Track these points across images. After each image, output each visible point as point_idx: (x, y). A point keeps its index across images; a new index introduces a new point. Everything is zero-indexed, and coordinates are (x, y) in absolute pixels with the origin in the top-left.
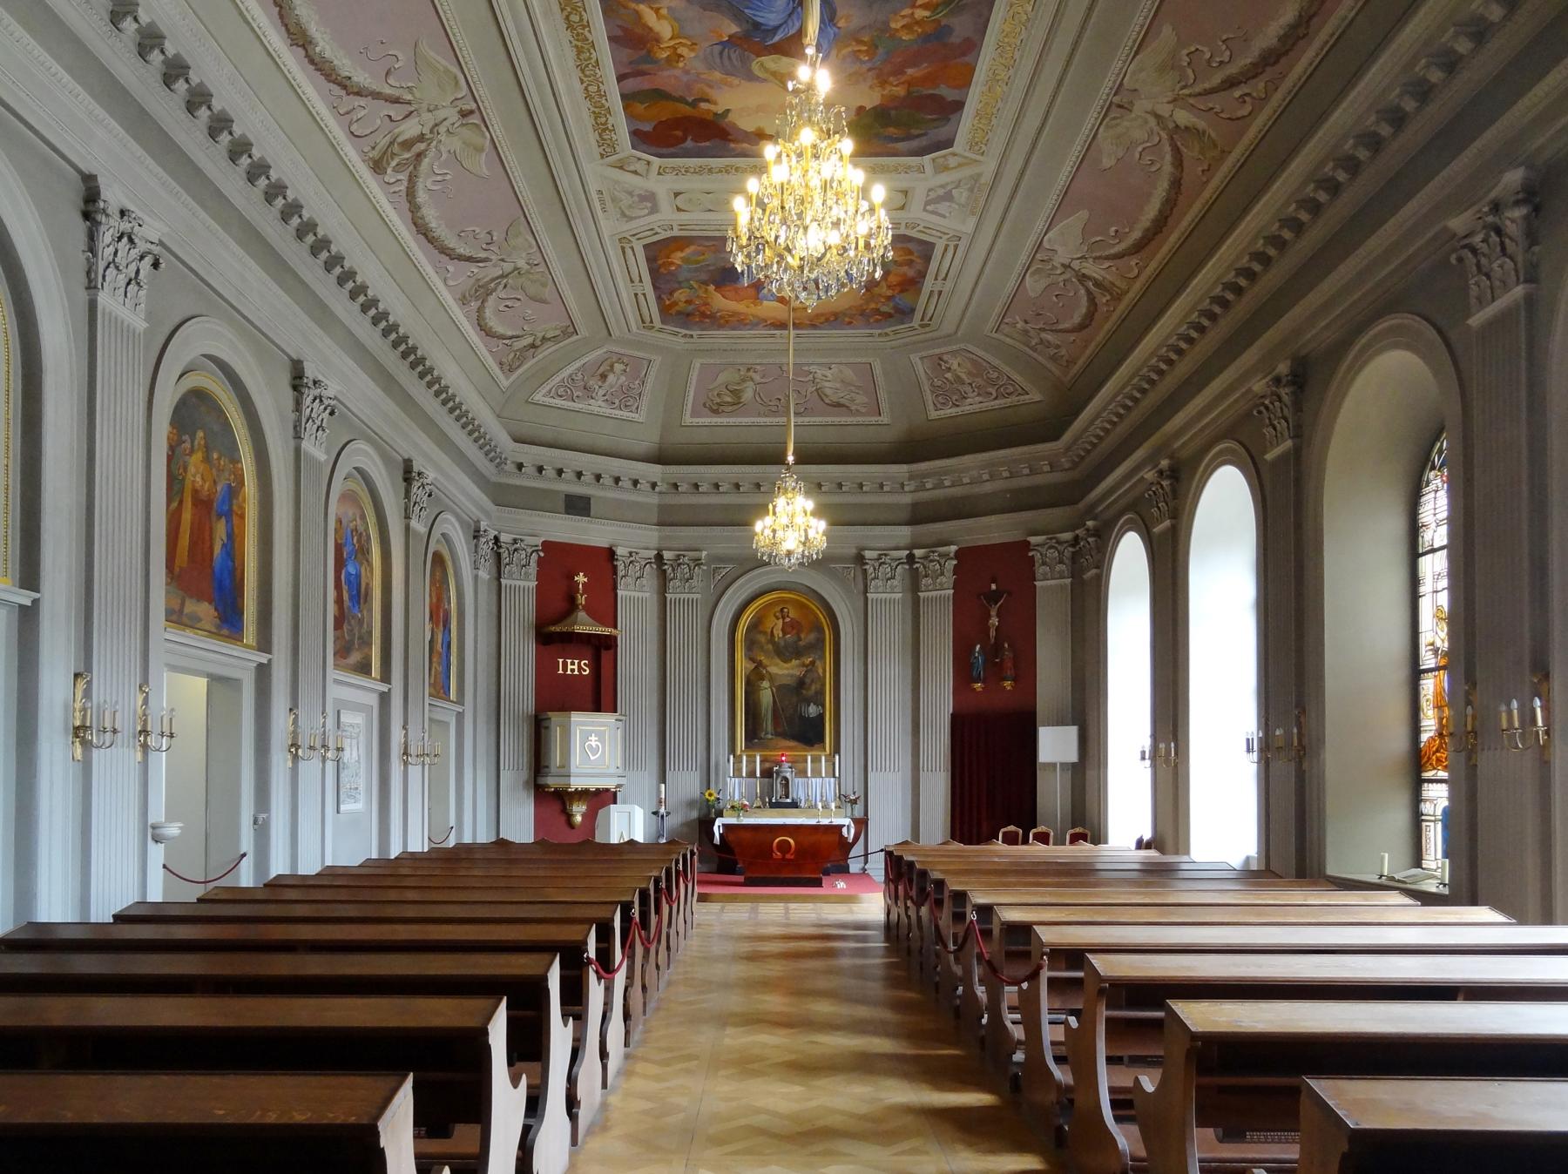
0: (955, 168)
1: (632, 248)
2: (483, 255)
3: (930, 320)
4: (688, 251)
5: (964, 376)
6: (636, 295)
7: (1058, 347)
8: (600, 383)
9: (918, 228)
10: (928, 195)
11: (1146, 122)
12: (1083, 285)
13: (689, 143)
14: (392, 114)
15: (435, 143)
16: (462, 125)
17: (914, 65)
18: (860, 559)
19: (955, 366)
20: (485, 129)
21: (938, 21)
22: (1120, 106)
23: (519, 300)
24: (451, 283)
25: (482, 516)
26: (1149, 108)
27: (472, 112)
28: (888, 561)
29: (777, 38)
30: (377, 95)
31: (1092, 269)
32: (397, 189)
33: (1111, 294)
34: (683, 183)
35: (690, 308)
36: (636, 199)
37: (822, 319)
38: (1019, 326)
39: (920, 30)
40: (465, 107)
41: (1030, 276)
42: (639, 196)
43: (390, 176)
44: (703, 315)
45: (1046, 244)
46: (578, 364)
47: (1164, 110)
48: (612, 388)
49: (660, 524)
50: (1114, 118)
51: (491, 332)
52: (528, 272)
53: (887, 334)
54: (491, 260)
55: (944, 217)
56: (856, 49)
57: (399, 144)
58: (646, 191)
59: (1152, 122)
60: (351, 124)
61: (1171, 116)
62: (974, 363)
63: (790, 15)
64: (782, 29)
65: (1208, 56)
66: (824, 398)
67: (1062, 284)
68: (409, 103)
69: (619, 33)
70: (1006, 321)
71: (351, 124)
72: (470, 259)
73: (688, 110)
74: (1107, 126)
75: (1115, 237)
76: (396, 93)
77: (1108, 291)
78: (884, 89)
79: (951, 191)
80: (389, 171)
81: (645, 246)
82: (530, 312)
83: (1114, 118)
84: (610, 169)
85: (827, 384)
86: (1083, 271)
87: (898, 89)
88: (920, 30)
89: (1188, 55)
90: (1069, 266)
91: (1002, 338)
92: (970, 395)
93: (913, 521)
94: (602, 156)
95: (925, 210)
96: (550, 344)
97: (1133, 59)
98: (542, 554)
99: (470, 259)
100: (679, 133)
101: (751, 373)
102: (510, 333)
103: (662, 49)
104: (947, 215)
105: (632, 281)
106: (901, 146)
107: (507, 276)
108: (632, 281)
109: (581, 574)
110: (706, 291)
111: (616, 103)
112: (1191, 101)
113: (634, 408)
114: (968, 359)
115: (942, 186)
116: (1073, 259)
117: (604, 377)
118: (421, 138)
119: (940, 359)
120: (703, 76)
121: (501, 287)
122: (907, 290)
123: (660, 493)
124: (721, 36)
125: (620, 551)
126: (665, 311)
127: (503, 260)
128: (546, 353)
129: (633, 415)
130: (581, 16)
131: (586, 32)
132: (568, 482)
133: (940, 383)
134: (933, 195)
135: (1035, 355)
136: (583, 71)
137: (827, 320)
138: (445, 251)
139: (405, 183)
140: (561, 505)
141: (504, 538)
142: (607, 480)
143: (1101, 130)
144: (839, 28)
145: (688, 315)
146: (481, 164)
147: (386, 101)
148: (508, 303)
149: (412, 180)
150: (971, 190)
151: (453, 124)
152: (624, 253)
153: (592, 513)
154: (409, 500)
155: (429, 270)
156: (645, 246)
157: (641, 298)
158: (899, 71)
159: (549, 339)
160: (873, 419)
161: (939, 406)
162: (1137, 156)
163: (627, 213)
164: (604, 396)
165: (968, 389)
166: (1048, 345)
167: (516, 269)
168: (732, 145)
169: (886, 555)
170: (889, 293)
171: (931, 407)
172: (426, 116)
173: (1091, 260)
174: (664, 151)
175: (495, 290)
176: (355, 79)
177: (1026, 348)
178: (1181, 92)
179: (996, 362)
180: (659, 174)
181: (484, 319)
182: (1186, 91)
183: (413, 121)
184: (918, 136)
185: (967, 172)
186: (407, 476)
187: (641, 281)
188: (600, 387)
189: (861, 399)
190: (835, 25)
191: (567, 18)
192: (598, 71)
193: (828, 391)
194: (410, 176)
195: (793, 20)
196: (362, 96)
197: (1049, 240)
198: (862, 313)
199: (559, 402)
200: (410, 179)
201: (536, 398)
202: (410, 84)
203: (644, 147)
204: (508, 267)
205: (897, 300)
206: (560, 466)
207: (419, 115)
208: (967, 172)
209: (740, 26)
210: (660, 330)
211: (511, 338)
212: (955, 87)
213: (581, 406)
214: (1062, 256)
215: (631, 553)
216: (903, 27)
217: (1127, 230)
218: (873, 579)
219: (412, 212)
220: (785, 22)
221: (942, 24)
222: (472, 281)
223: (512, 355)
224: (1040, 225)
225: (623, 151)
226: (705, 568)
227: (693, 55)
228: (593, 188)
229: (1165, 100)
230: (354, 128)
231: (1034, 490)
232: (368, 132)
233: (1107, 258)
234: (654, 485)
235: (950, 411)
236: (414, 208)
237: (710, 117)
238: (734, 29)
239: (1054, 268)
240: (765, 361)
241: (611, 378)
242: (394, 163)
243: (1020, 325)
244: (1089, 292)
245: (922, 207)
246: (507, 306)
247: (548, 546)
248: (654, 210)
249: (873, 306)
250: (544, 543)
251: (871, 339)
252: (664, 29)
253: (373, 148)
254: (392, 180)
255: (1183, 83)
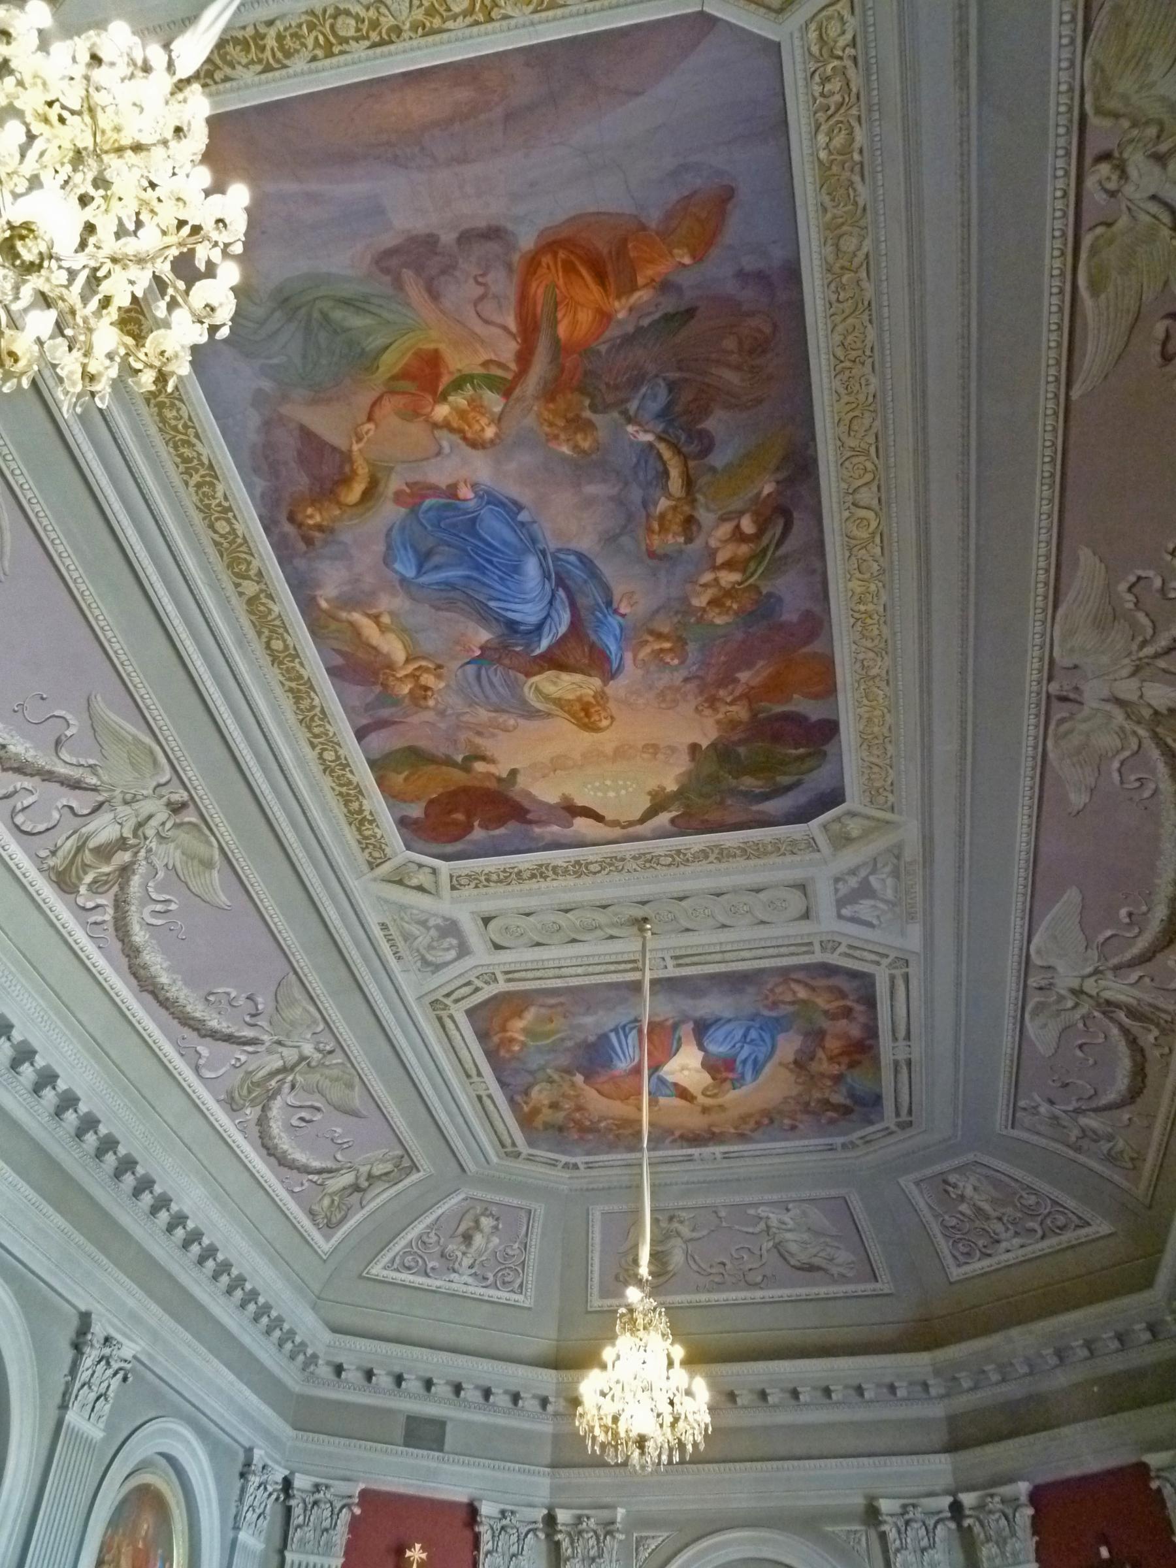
0: (860, 837)
1: (451, 1017)
2: (249, 1033)
3: (910, 1112)
4: (530, 1015)
5: (986, 1207)
6: (480, 1098)
7: (1110, 1138)
8: (463, 1248)
9: (840, 950)
10: (836, 890)
11: (1109, 716)
12: (1112, 1019)
13: (478, 834)
14: (74, 804)
15: (142, 853)
16: (176, 826)
17: (749, 665)
18: (872, 1514)
19: (969, 1192)
20: (207, 832)
21: (755, 588)
22: (1064, 699)
23: (318, 1109)
24: (208, 1074)
25: (259, 1441)
26: (1105, 693)
27: (184, 805)
28: (919, 1516)
29: (545, 643)
30: (48, 776)
31: (1118, 990)
32: (99, 918)
33: (1158, 1025)
34: (495, 900)
35: (560, 1116)
36: (433, 932)
37: (752, 1124)
38: (1042, 1110)
39: (735, 606)
40: (175, 798)
41: (1032, 1019)
42: (437, 927)
43: (84, 898)
44: (583, 1130)
45: (1036, 960)
46: (429, 1219)
47: (1128, 689)
48: (480, 1255)
49: (553, 1466)
50: (1062, 721)
51: (285, 1157)
52: (321, 1064)
53: (854, 1145)
54: (262, 1043)
55: (869, 924)
56: (657, 646)
57: (91, 850)
58: (445, 919)
59: (1119, 715)
60: (13, 813)
61: (1141, 697)
62: (997, 1184)
63: (551, 603)
64: (546, 629)
65: (1158, 583)
66: (789, 1258)
67: (1081, 1025)
68: (94, 789)
69: (339, 661)
70: (1022, 1103)
71: (13, 813)
72: (229, 1039)
73: (458, 777)
74: (1058, 738)
75: (1131, 924)
76: (76, 773)
77: (1151, 1021)
78: (716, 710)
79: (866, 879)
80: (83, 889)
81: (470, 1013)
82: (339, 1130)
83: (1062, 721)
84: (389, 886)
85: (789, 1236)
86: (1107, 995)
87: (733, 708)
88: (735, 606)
89: (1130, 589)
90: (1082, 992)
91: (1025, 1135)
92: (1003, 1236)
93: (953, 1446)
94: (372, 866)
95: (840, 917)
96: (379, 1187)
97: (1053, 618)
98: (357, 1511)
99: (229, 1039)
100: (460, 816)
101: (675, 1225)
102: (316, 1164)
103: (400, 679)
104: (875, 922)
105: (468, 1076)
106: (772, 807)
107: (292, 1069)
108: (468, 1076)
109: (418, 1546)
110: (573, 1085)
111: (365, 776)
112: (1162, 663)
113: (516, 1285)
114: (987, 1177)
115: (853, 872)
116: (1083, 978)
117: (467, 1238)
118: (122, 844)
119: (946, 1182)
120: (465, 718)
121: (286, 1088)
122: (859, 1063)
123: (556, 1414)
124: (471, 650)
125: (487, 1509)
126: (526, 1121)
127: (279, 1043)
128: (379, 1201)
129: (516, 1297)
130: (284, 641)
131: (296, 664)
132: (411, 1396)
133: (953, 1222)
134: (843, 889)
135: (1082, 1158)
136: (309, 728)
137: (758, 1124)
138: (186, 1021)
139: (110, 911)
140: (399, 1433)
141: (301, 1482)
142: (471, 1394)
143: (1050, 744)
144: (623, 616)
145: (561, 1129)
146: (214, 883)
147: (62, 784)
148: (303, 1114)
149: (120, 905)
150: (896, 874)
151: (163, 824)
152: (443, 1027)
153: (447, 1447)
154: (74, 1379)
155: (168, 1050)
156: (470, 1013)
157: (487, 1102)
158: (727, 679)
159: (379, 1177)
160: (869, 1287)
161: (960, 1258)
162: (1116, 776)
163: (430, 958)
164: (471, 1267)
165: (999, 1227)
166: (1096, 1137)
167: (303, 1058)
168: (537, 830)
169: (914, 1506)
170: (835, 1069)
171: (950, 1261)
172: (123, 810)
173: (1110, 975)
174: (449, 849)
175: (277, 1091)
176: (11, 748)
177: (1065, 1149)
178: (1141, 654)
179: (1029, 1179)
180: (453, 888)
181: (271, 1138)
182: (1149, 650)
183: (105, 817)
184: (789, 788)
185: (880, 843)
186: (246, 1469)
187: (479, 1074)
188: (464, 1254)
189: (843, 1256)
190: (616, 611)
191: (268, 646)
192: (328, 727)
193: (793, 1248)
194: (116, 900)
195: (557, 611)
196: (25, 774)
197: (1038, 952)
198: (806, 1109)
199: (405, 1277)
200: (117, 907)
201: (374, 1271)
202: (91, 762)
203: (420, 844)
204: (291, 1055)
205: (849, 1080)
206: (397, 1369)
207: (113, 809)
208: (880, 843)
209: (488, 628)
210: (530, 1159)
211: (319, 1172)
212: (816, 696)
213: (438, 1283)
214: (1066, 979)
215: (503, 1512)
216: (709, 603)
217: (1144, 908)
218: (898, 1550)
219: (128, 956)
220: (548, 615)
221: (764, 592)
222: (240, 1074)
223: (326, 1202)
224: (1016, 925)
225: (396, 855)
226: (622, 1537)
227: (442, 685)
228: (373, 921)
229: (1125, 672)
230: (19, 819)
231: (1136, 1375)
232: (41, 827)
233: (1132, 964)
234: (544, 1402)
235: (979, 1265)
236: (131, 952)
237: (492, 785)
238: (484, 636)
239: (1061, 998)
240: (690, 1203)
241: (478, 1240)
242: (88, 879)
243: (1044, 1109)
244: (1125, 1031)
245: (835, 914)
246: (302, 1119)
247: (367, 1496)
248: (464, 950)
249: (817, 1095)
250: (364, 1494)
251: (830, 1155)
252: (394, 647)
253: (54, 853)
254: (90, 905)
255: (1141, 639)
